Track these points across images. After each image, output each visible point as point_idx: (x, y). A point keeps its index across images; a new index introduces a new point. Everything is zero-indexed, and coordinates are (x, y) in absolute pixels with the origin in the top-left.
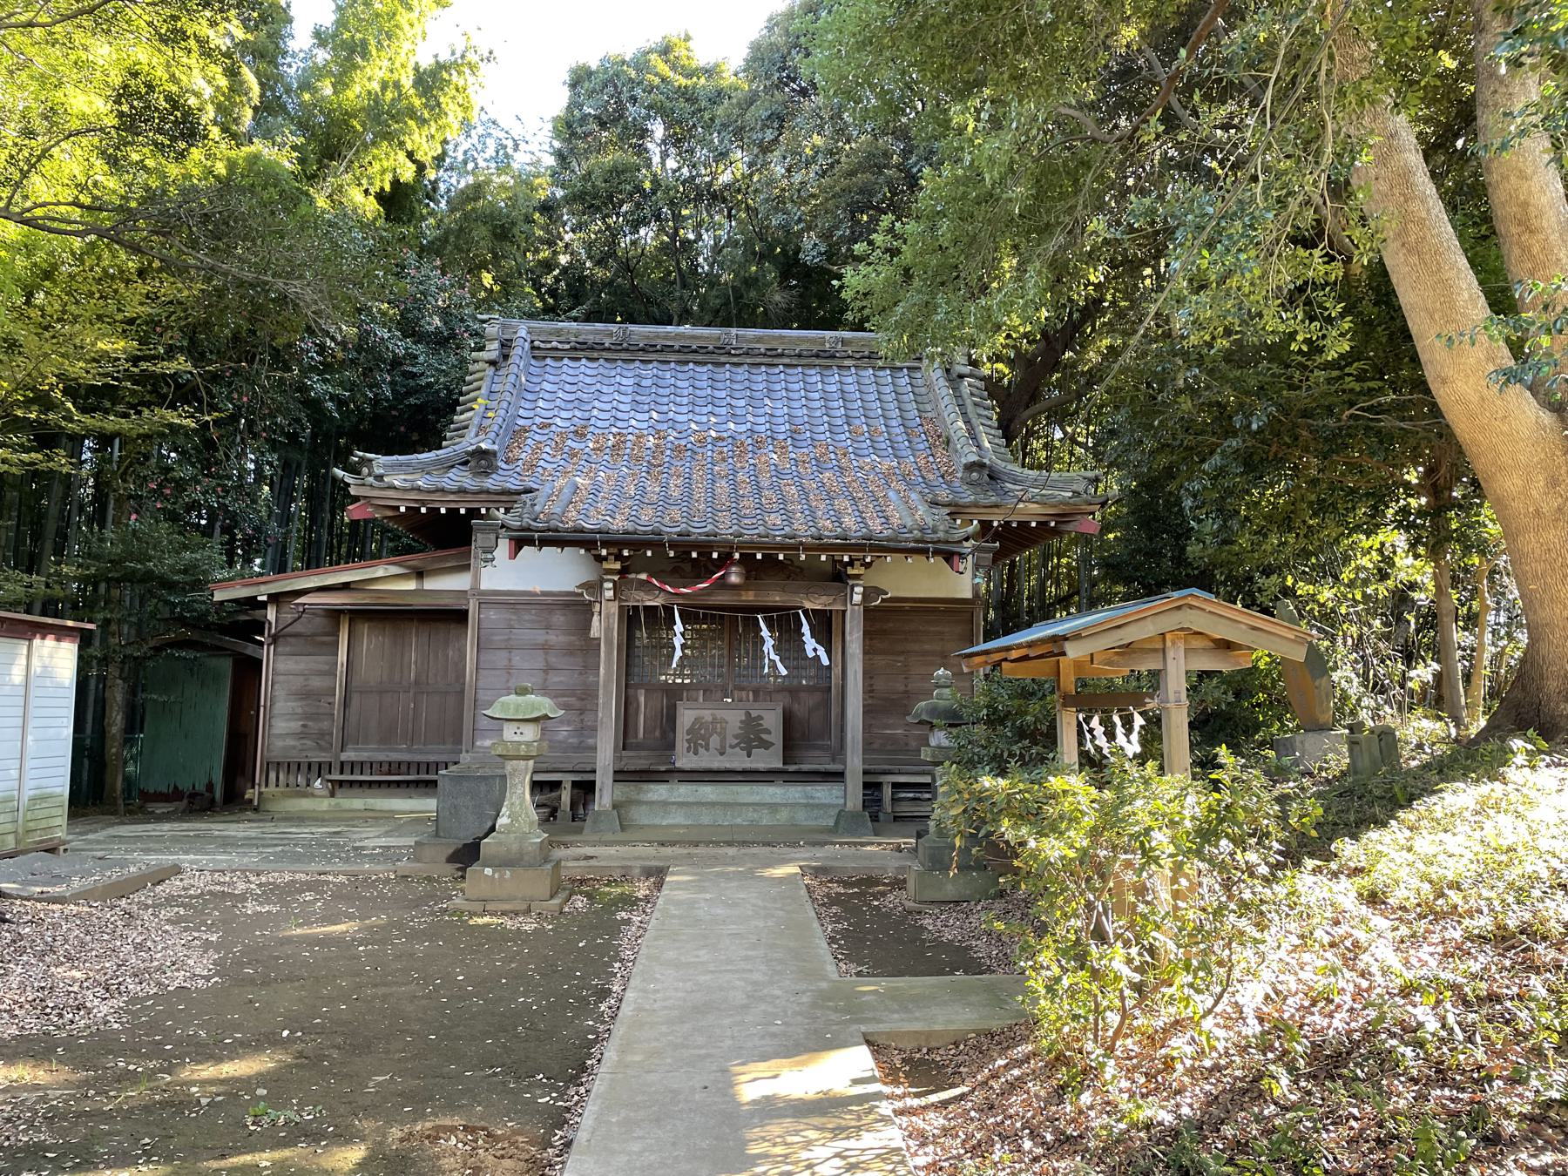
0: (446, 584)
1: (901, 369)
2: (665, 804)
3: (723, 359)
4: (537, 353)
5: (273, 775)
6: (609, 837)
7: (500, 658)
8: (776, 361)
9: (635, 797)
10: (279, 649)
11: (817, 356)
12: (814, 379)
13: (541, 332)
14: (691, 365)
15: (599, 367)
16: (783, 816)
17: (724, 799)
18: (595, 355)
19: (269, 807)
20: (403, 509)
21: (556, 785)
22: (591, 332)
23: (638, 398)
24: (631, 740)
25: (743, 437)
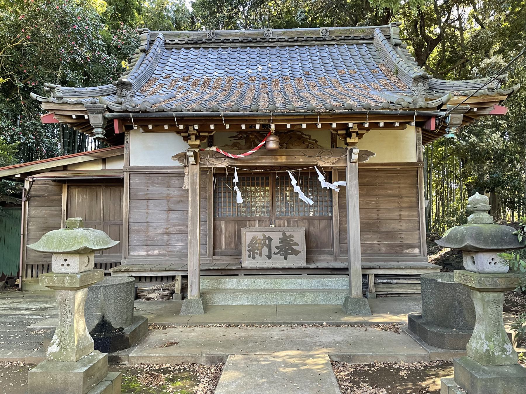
0: (115, 167)
1: (362, 44)
2: (235, 291)
3: (265, 44)
4: (167, 46)
5: (29, 271)
6: (197, 319)
7: (142, 204)
8: (294, 44)
9: (216, 285)
10: (32, 204)
11: (316, 40)
12: (315, 51)
13: (170, 36)
14: (248, 48)
15: (201, 51)
16: (309, 299)
17: (271, 287)
18: (198, 46)
19: (27, 288)
20: (74, 117)
21: (173, 277)
22: (196, 35)
23: (219, 63)
24: (218, 250)
25: (277, 78)
